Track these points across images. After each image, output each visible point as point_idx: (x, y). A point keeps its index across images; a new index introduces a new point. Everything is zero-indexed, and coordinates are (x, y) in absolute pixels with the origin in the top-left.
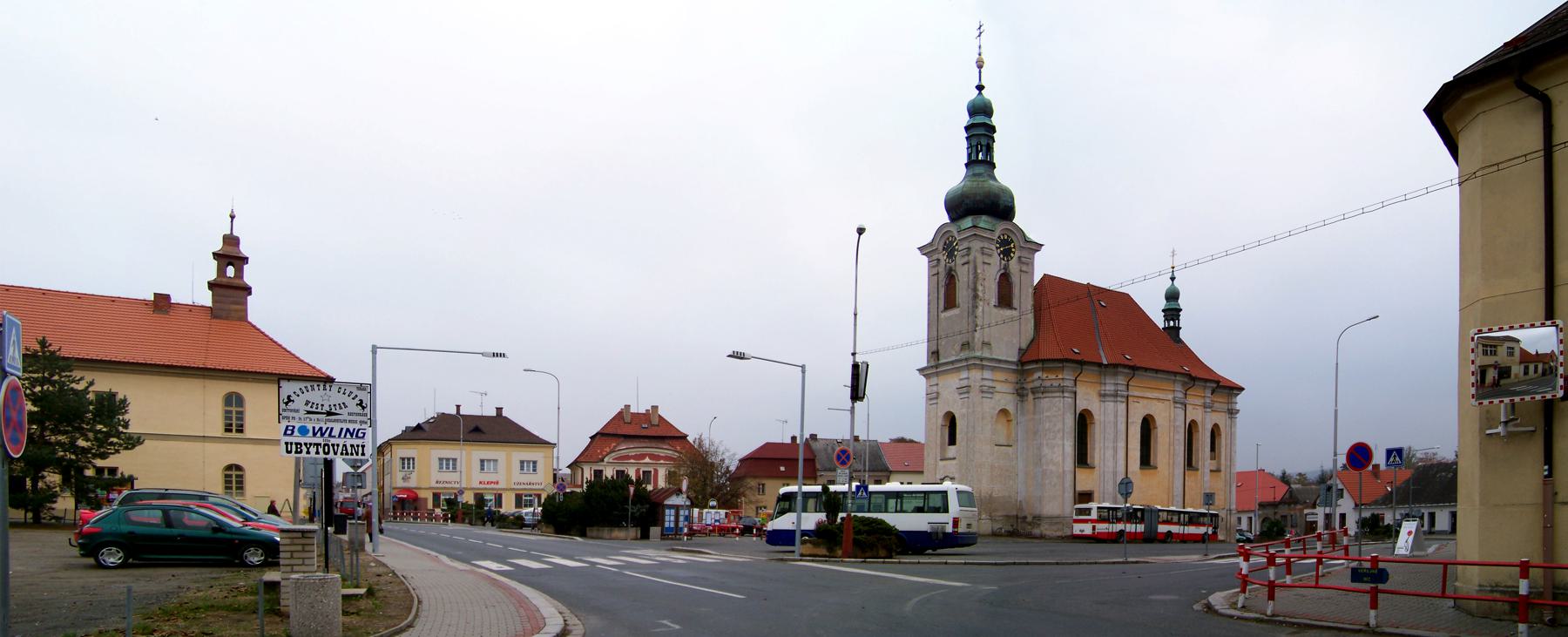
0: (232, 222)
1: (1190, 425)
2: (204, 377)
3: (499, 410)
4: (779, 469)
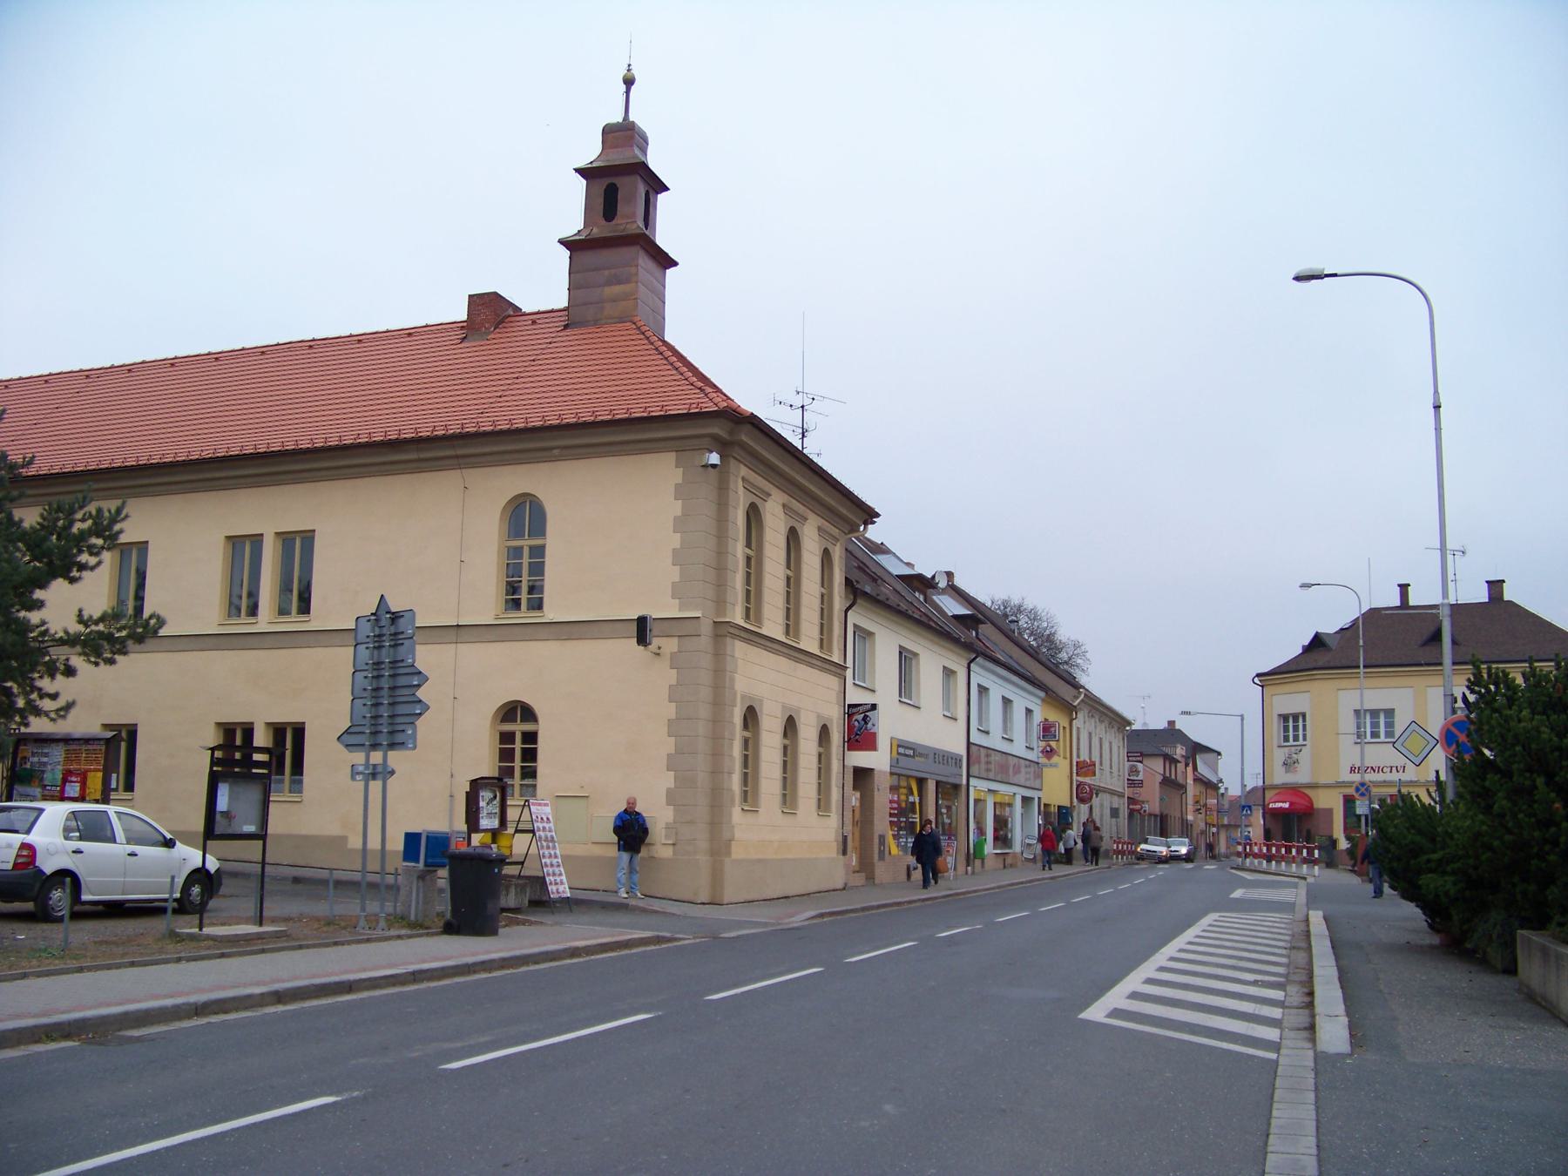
0: (628, 92)
1: (1078, 786)
2: (461, 462)
3: (1495, 586)
4: (234, 755)
